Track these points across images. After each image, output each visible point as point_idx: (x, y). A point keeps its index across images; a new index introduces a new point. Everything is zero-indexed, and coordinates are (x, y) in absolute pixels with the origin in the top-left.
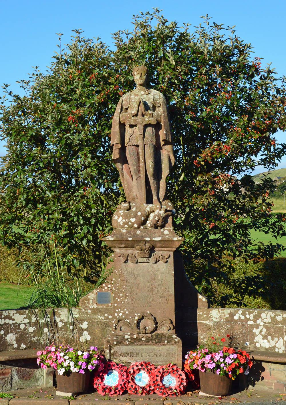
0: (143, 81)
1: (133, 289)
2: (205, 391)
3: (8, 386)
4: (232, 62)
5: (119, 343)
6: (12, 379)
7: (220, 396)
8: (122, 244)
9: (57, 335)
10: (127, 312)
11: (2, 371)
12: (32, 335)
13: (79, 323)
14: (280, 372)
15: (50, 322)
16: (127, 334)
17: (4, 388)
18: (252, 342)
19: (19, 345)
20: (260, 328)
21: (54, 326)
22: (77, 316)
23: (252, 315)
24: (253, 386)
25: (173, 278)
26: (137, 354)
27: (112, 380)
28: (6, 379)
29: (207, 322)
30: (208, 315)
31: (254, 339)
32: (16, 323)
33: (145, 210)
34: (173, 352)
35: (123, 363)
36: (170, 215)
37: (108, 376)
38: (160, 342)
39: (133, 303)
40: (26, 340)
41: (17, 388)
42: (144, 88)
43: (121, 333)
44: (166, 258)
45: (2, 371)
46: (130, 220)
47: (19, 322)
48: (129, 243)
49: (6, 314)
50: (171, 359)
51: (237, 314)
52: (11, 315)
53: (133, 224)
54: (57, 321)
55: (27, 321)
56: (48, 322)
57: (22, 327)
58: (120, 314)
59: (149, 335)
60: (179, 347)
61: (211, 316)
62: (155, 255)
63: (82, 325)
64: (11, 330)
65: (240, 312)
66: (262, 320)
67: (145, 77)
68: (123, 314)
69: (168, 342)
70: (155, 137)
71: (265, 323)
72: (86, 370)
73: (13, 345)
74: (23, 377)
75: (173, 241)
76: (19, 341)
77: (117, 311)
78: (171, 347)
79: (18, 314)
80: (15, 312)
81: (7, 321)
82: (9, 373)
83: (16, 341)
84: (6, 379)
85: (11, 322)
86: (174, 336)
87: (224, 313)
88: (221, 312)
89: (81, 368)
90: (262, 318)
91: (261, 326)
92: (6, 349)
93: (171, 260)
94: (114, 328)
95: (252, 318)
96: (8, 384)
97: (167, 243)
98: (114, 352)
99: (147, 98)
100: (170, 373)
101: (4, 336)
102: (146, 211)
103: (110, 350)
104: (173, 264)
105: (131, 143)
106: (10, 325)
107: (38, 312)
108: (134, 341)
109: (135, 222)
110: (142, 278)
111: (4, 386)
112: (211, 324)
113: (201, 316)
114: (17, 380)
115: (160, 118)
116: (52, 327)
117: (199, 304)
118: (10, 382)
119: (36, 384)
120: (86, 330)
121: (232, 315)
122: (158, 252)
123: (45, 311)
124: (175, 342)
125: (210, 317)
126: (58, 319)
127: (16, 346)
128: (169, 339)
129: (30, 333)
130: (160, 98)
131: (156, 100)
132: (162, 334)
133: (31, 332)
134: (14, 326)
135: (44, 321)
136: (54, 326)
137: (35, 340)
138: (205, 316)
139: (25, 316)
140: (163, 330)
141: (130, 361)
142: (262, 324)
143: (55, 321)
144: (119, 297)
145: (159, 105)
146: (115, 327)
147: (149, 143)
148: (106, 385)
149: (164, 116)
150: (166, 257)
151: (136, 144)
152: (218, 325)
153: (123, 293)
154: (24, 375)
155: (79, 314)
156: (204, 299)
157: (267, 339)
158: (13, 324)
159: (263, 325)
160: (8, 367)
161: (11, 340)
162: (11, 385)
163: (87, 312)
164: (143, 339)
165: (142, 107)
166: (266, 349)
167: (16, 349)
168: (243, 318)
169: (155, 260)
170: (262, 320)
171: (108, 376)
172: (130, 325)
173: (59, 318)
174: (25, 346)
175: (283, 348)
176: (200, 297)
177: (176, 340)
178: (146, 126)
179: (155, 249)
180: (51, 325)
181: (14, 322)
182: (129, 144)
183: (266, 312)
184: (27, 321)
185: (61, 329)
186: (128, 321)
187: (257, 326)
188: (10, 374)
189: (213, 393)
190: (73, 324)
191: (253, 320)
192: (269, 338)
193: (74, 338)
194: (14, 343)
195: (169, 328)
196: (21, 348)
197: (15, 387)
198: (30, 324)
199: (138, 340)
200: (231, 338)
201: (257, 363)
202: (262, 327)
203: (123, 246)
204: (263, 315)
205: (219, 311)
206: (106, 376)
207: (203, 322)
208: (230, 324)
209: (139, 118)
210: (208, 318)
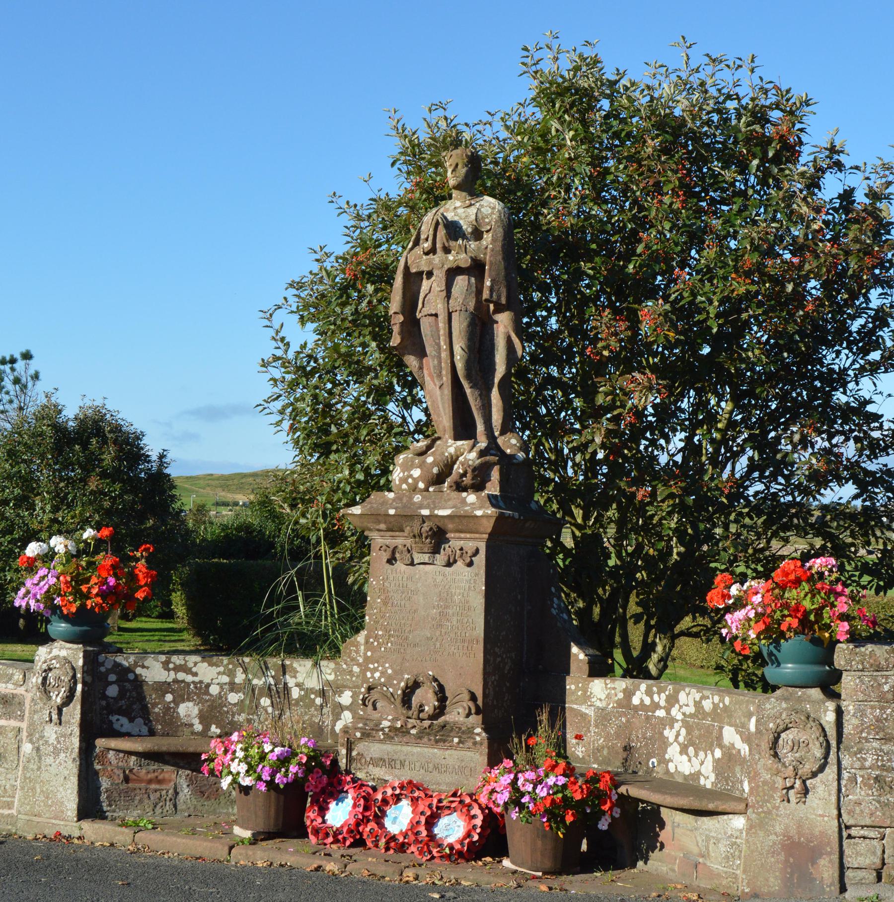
0: (459, 179)
1: (403, 622)
2: (513, 862)
3: (167, 808)
4: (738, 149)
5: (366, 735)
6: (176, 793)
7: (540, 874)
8: (379, 522)
9: (288, 714)
10: (390, 671)
11: (156, 774)
12: (235, 709)
13: (335, 693)
14: (688, 832)
15: (275, 685)
16: (386, 719)
17: (158, 810)
18: (664, 762)
19: (207, 728)
20: (677, 726)
21: (282, 695)
22: (331, 678)
23: (663, 696)
24: (646, 863)
25: (483, 601)
26: (402, 764)
27: (339, 814)
28: (164, 793)
29: (583, 709)
30: (585, 691)
31: (665, 752)
32: (201, 682)
33: (443, 453)
34: (473, 765)
35: (374, 779)
36: (495, 464)
37: (337, 804)
38: (444, 741)
39: (402, 651)
40: (222, 719)
41: (186, 814)
42: (464, 194)
43: (375, 715)
44: (469, 555)
45: (156, 774)
46: (412, 472)
47: (207, 680)
48: (392, 520)
49: (178, 662)
50: (467, 780)
51: (638, 693)
52: (190, 665)
53: (416, 481)
54: (289, 685)
55: (225, 679)
56: (270, 685)
57: (214, 690)
58: (377, 675)
59: (427, 723)
60: (481, 754)
61: (591, 693)
62: (447, 548)
63: (340, 696)
64: (189, 694)
65: (643, 687)
66: (681, 707)
67: (464, 170)
68: (383, 673)
69: (460, 742)
70: (473, 295)
71: (684, 714)
72: (271, 784)
73: (192, 725)
74: (203, 793)
75: (477, 517)
76: (205, 719)
77: (371, 666)
78: (469, 753)
79: (206, 664)
80: (197, 658)
81: (181, 676)
82: (170, 781)
83: (200, 718)
84: (164, 793)
85: (189, 678)
86: (478, 730)
87: (614, 688)
88: (609, 686)
89: (259, 778)
90: (681, 704)
91: (677, 721)
92: (176, 732)
93: (480, 560)
94: (360, 702)
95: (663, 703)
96: (168, 803)
97: (464, 521)
98: (358, 754)
99: (463, 215)
100: (455, 810)
101: (172, 705)
102: (446, 454)
103: (349, 750)
104: (484, 568)
105: (426, 311)
106: (188, 684)
107: (248, 663)
108: (398, 733)
109: (420, 478)
110: (421, 599)
111: (158, 807)
112: (590, 712)
113: (573, 693)
114: (188, 797)
115: (485, 254)
116: (279, 697)
117: (573, 667)
118: (171, 800)
119: (230, 810)
120: (347, 708)
121: (629, 694)
122: (455, 542)
123: (265, 663)
124: (475, 743)
125: (589, 697)
126: (291, 682)
127: (198, 727)
128: (466, 734)
129: (230, 704)
130: (492, 213)
131: (483, 218)
132: (455, 723)
133: (233, 702)
134: (196, 688)
135: (261, 683)
136: (282, 695)
137: (241, 719)
138: (580, 693)
139: (221, 669)
140: (456, 715)
141: (387, 778)
142: (680, 717)
143: (286, 684)
144: (376, 638)
145: (489, 228)
146: (364, 700)
147: (458, 308)
148: (328, 822)
149: (492, 250)
150: (470, 553)
151: (434, 313)
152: (603, 716)
153: (386, 631)
154: (203, 789)
155: (336, 674)
156: (582, 656)
157: (687, 754)
158: (193, 682)
159: (682, 721)
160: (168, 768)
161: (189, 716)
162: (175, 806)
163: (352, 671)
164: (413, 731)
165: (442, 232)
166: (686, 777)
167: (197, 734)
168: (647, 701)
169: (446, 559)
170: (681, 707)
171: (337, 804)
172: (392, 700)
173: (294, 679)
174: (218, 731)
175: (712, 777)
176: (575, 649)
177: (478, 739)
178: (453, 273)
179: (447, 536)
180: (278, 692)
181: (196, 679)
182: (423, 314)
183: (687, 690)
184: (225, 679)
185: (297, 701)
186: (391, 690)
187: (672, 721)
188: (172, 783)
189: (523, 864)
190: (322, 693)
191: (664, 708)
192: (691, 750)
193: (323, 722)
194: (196, 721)
195: (467, 711)
196: (210, 734)
197: (182, 810)
198: (233, 687)
199: (403, 731)
200: (627, 748)
201: (653, 809)
202: (680, 723)
203: (383, 526)
204: (682, 696)
205: (606, 684)
206: (332, 805)
207: (575, 706)
208: (625, 716)
209: (437, 259)
210: (586, 698)
